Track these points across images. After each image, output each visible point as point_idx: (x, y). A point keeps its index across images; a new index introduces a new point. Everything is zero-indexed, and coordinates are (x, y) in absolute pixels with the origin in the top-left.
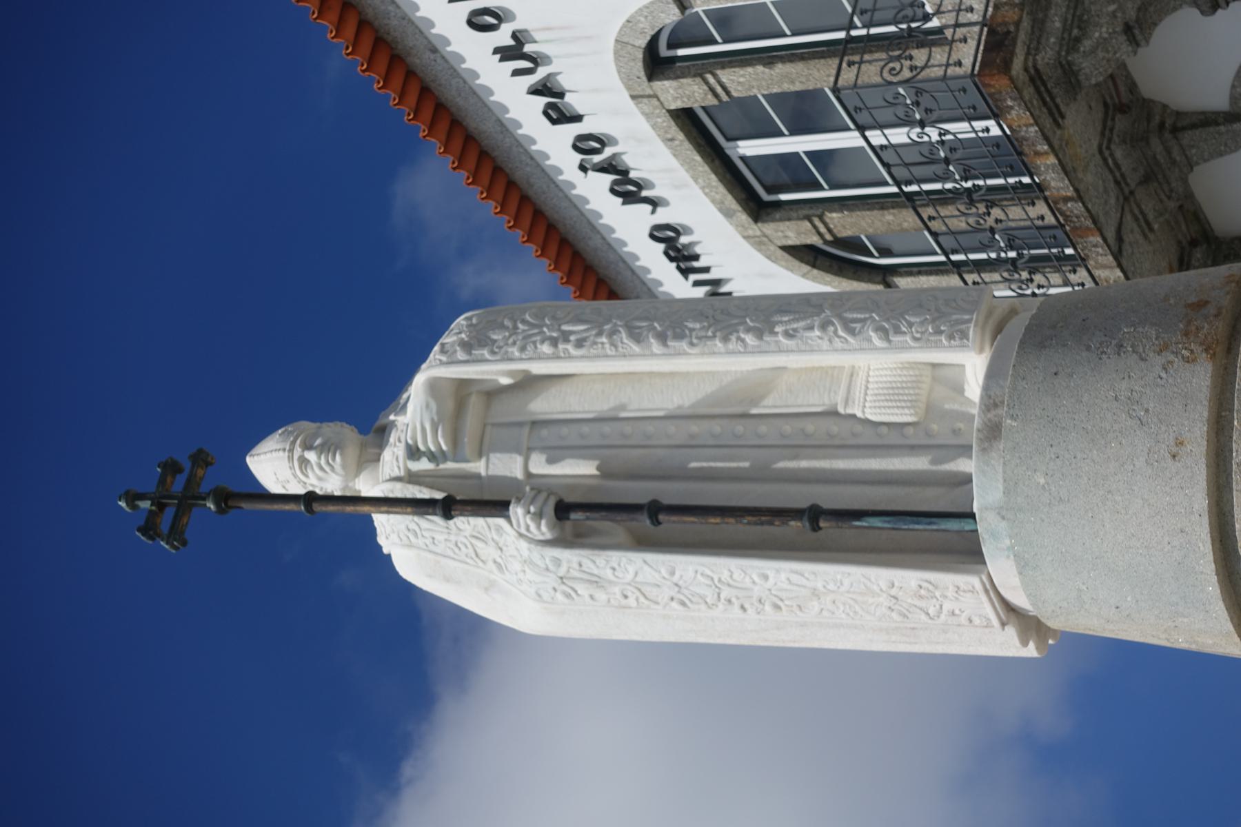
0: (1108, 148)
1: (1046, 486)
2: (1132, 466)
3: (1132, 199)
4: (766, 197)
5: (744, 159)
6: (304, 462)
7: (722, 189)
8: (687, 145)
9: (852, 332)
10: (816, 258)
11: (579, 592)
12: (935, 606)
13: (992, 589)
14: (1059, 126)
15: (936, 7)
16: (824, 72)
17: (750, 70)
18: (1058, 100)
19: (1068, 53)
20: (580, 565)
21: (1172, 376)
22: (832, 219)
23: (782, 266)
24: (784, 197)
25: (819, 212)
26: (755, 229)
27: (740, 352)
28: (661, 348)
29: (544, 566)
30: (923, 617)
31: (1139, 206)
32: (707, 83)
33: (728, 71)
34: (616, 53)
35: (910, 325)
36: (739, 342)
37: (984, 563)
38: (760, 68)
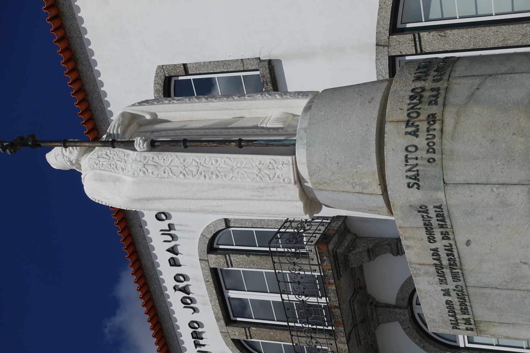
0: (353, 302)
3: (355, 324)
4: (232, 318)
5: (229, 298)
7: (219, 308)
8: (212, 285)
10: (242, 349)
12: (273, 174)
13: (295, 164)
14: (338, 278)
15: (308, 240)
16: (265, 262)
17: (241, 256)
18: (340, 269)
19: (347, 253)
20: (153, 159)
22: (252, 330)
23: (230, 349)
24: (238, 319)
25: (249, 327)
26: (225, 329)
29: (140, 160)
31: (358, 331)
32: (226, 259)
33: (235, 255)
34: (200, 239)
38: (245, 256)
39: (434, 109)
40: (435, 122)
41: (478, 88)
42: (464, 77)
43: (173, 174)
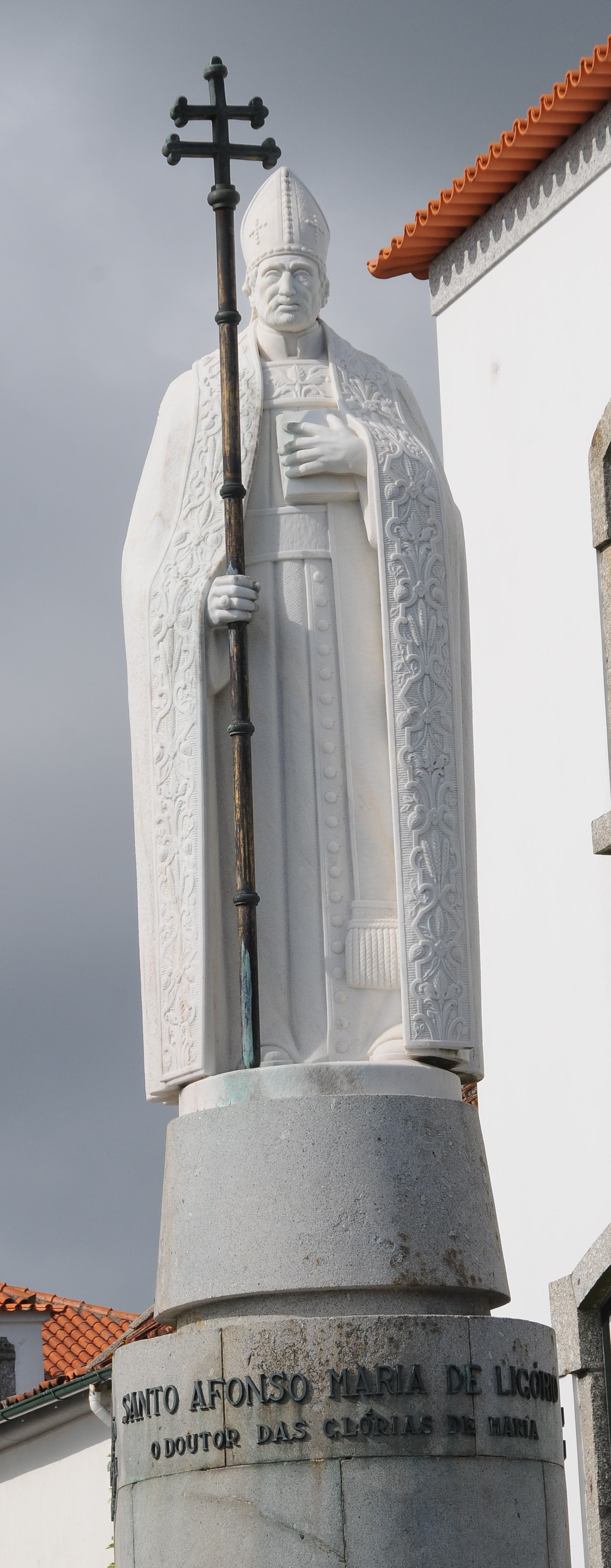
1: (278, 1141)
2: (298, 1221)
6: (277, 271)
9: (422, 921)
11: (161, 643)
21: (378, 1249)
27: (399, 808)
28: (401, 722)
30: (165, 1007)
35: (430, 979)
36: (409, 805)
37: (218, 1072)
39: (249, 1440)
40: (223, 1446)
41: (303, 1538)
42: (342, 1494)
43: (160, 721)
